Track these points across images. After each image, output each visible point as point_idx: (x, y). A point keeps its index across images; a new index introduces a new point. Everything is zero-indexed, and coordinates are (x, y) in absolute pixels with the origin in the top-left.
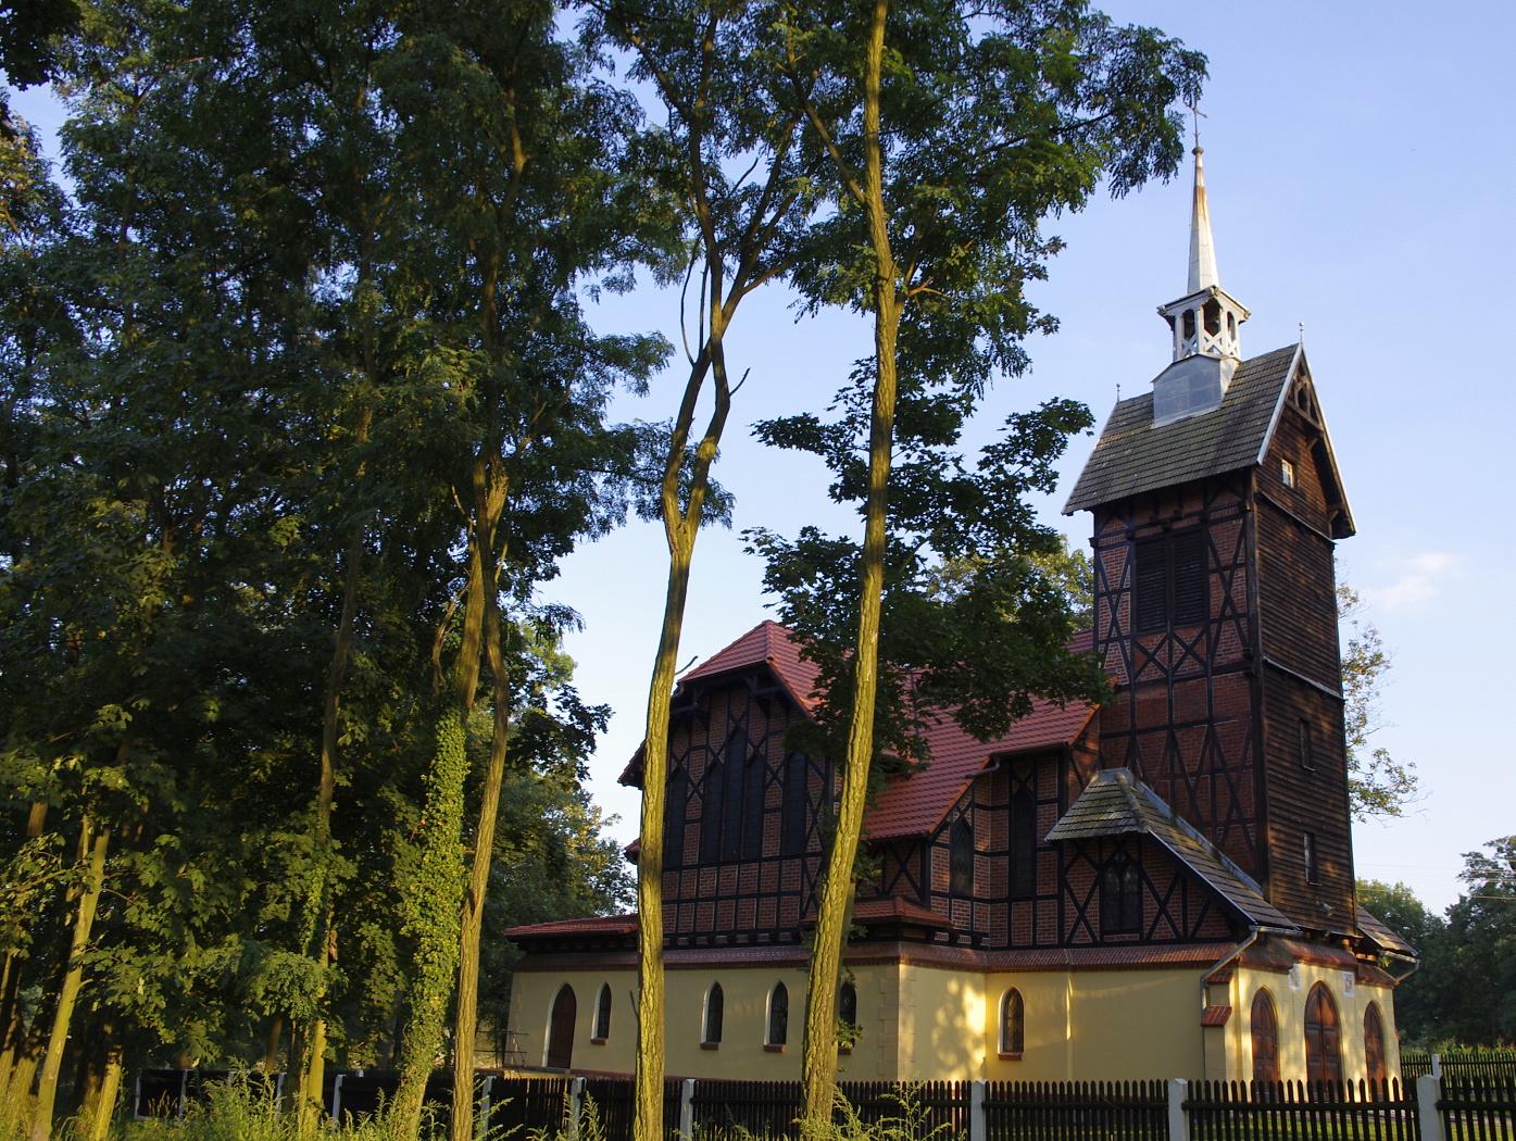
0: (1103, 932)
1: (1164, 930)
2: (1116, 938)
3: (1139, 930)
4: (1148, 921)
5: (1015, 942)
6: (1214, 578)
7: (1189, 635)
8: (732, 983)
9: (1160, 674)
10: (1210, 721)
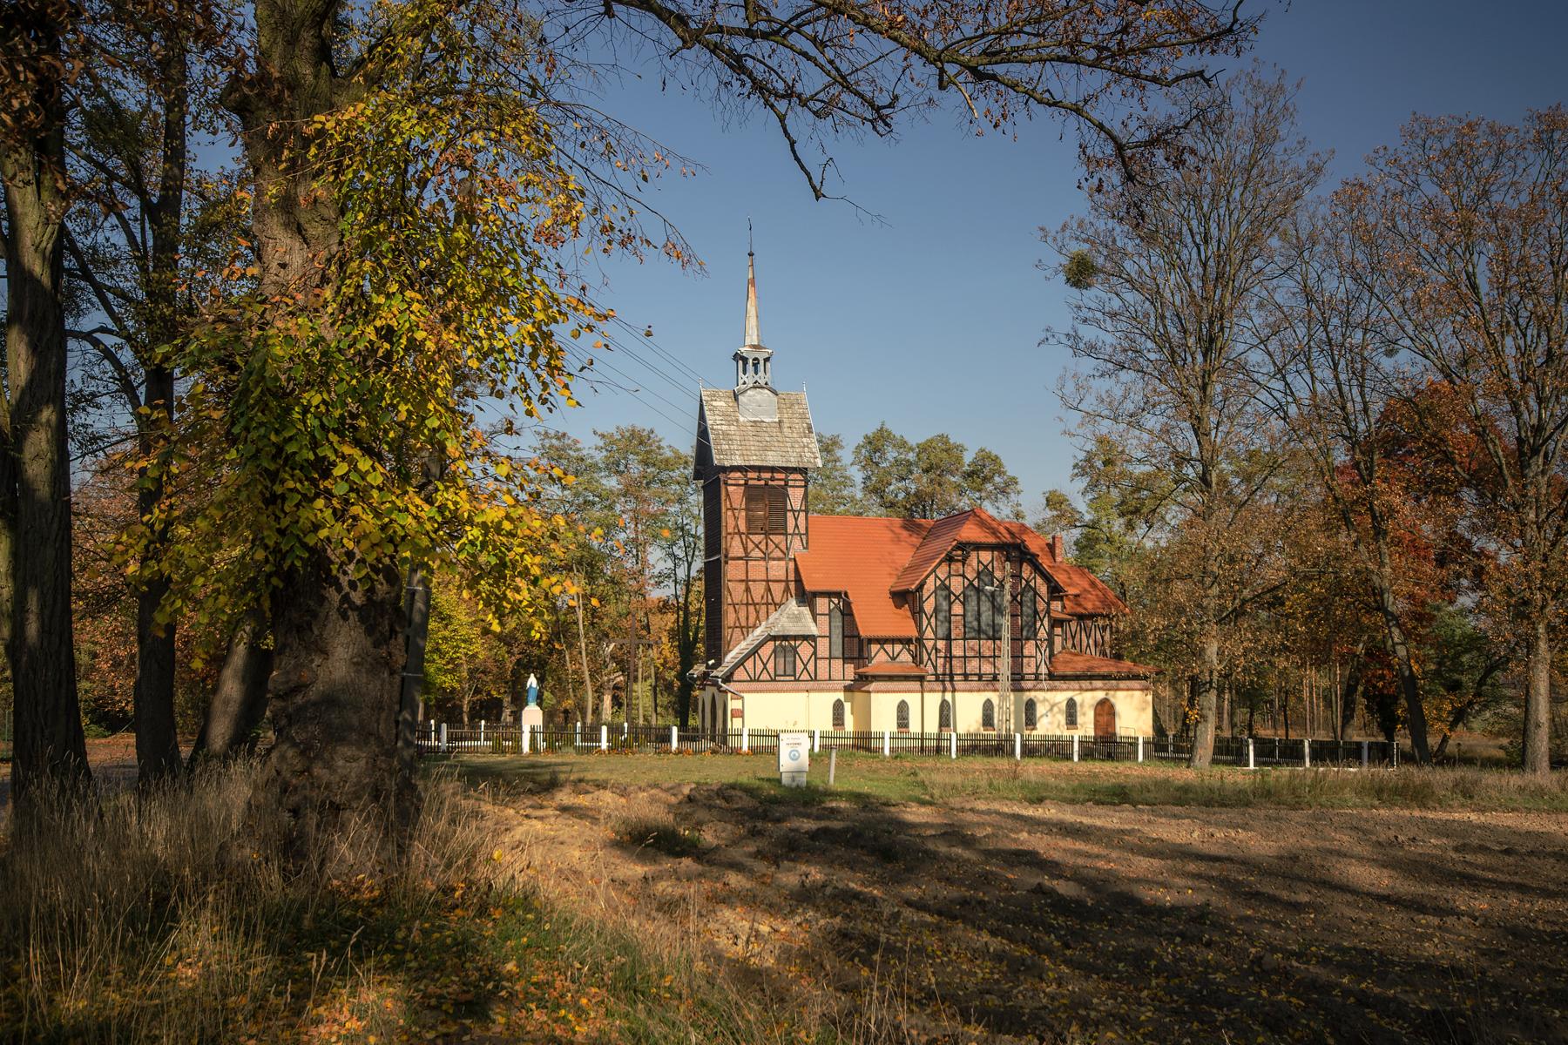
1: (765, 676)
6: (789, 514)
8: (908, 697)
9: (780, 555)
10: (768, 581)
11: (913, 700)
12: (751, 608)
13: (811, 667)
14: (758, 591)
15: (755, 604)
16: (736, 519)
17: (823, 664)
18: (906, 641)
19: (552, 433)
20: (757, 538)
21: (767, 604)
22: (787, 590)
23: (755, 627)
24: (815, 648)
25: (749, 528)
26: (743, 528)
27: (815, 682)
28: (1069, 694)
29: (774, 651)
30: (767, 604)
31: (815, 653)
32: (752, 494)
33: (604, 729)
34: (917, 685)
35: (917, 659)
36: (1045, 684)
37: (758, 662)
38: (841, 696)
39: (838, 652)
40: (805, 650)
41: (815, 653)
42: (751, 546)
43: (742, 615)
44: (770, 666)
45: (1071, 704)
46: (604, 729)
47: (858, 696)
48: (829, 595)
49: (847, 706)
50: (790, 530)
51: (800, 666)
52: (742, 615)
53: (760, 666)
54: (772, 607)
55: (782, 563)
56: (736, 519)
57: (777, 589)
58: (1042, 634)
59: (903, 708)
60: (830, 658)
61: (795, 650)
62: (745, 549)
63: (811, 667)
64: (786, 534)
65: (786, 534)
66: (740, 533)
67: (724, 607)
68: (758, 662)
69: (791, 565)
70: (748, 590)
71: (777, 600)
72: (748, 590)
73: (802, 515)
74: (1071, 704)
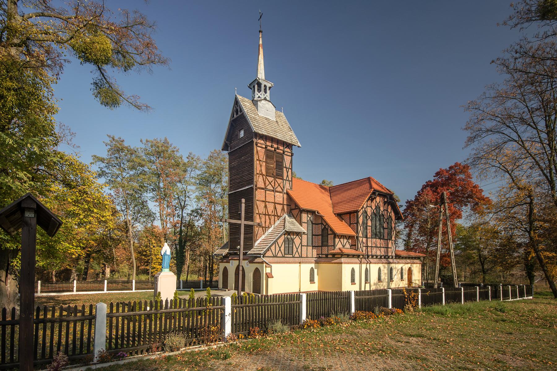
0: (285, 254)
1: (297, 255)
2: (287, 256)
3: (292, 254)
4: (294, 252)
5: (303, 256)
6: (285, 169)
7: (279, 181)
10: (275, 203)
11: (356, 267)
12: (267, 217)
13: (299, 250)
14: (271, 207)
15: (269, 215)
16: (261, 166)
17: (304, 249)
18: (350, 237)
19: (116, 138)
20: (271, 179)
21: (265, 215)
22: (283, 209)
23: (269, 228)
24: (301, 240)
25: (267, 173)
26: (264, 173)
27: (301, 259)
28: (409, 265)
29: (284, 241)
30: (274, 216)
31: (301, 243)
32: (269, 155)
33: (106, 281)
34: (356, 260)
35: (353, 246)
36: (395, 261)
37: (277, 246)
38: (313, 265)
39: (310, 244)
40: (297, 240)
41: (301, 243)
42: (267, 183)
43: (263, 220)
44: (282, 248)
45: (402, 269)
46: (106, 281)
47: (325, 266)
48: (308, 212)
49: (316, 271)
50: (285, 178)
51: (295, 250)
52: (263, 220)
53: (278, 249)
54: (276, 218)
55: (282, 194)
56: (261, 166)
57: (279, 208)
58: (393, 239)
59: (353, 271)
60: (307, 246)
61: (293, 240)
62: (265, 184)
63: (299, 250)
64: (283, 179)
65: (283, 179)
66: (263, 175)
67: (255, 215)
68: (277, 246)
69: (285, 196)
70: (266, 206)
71: (279, 214)
72: (266, 206)
73: (290, 170)
74: (402, 269)
